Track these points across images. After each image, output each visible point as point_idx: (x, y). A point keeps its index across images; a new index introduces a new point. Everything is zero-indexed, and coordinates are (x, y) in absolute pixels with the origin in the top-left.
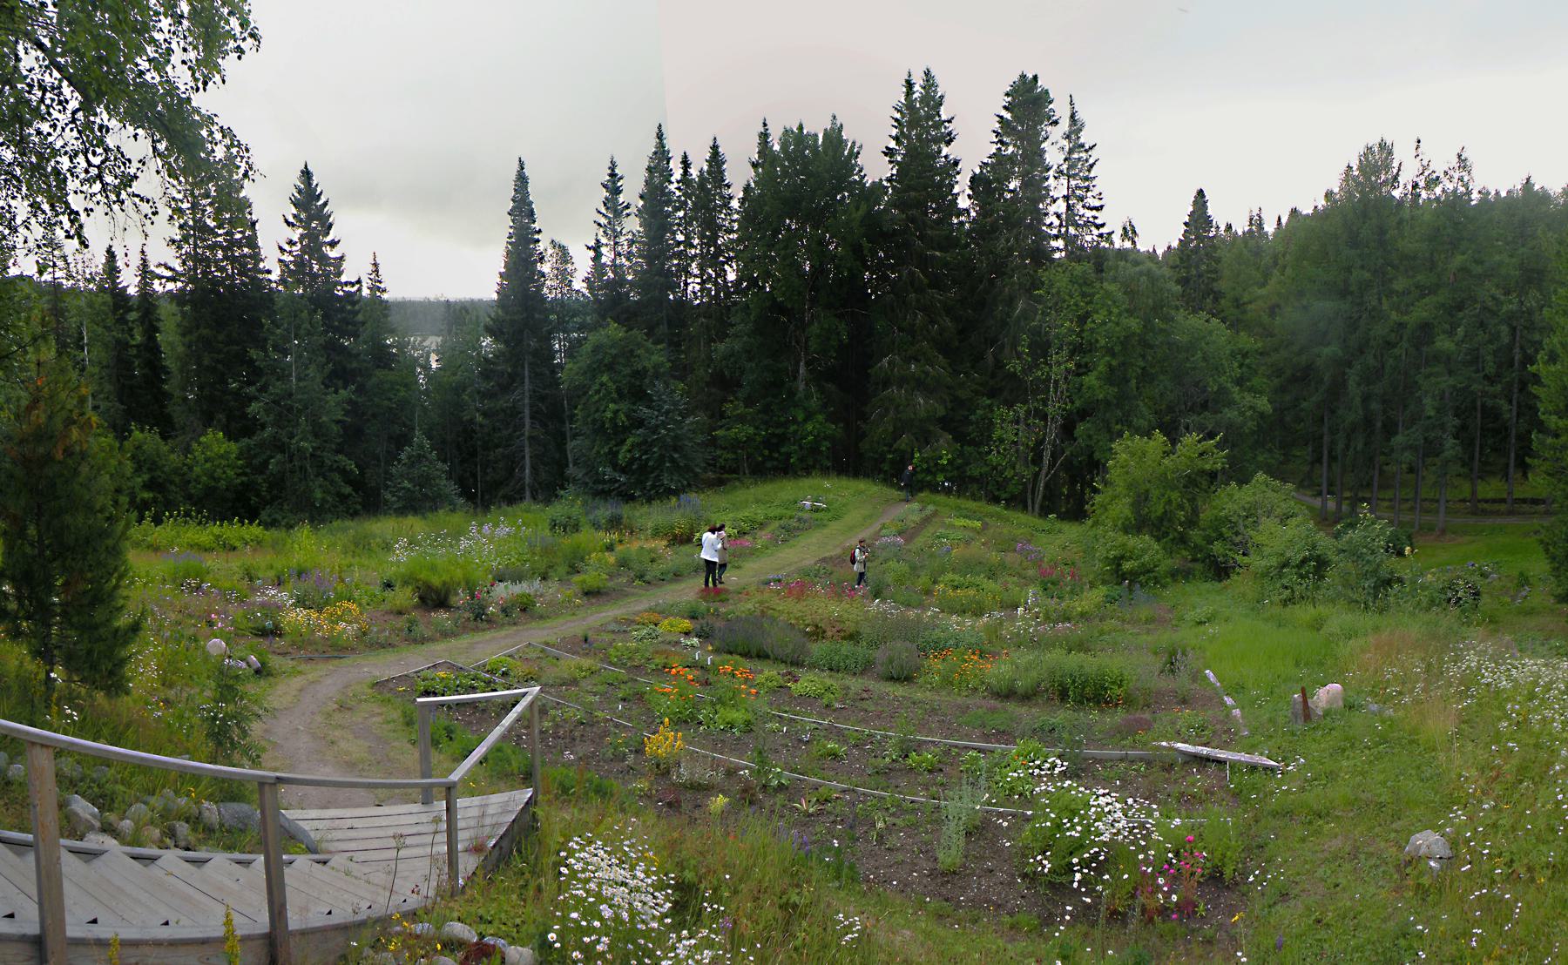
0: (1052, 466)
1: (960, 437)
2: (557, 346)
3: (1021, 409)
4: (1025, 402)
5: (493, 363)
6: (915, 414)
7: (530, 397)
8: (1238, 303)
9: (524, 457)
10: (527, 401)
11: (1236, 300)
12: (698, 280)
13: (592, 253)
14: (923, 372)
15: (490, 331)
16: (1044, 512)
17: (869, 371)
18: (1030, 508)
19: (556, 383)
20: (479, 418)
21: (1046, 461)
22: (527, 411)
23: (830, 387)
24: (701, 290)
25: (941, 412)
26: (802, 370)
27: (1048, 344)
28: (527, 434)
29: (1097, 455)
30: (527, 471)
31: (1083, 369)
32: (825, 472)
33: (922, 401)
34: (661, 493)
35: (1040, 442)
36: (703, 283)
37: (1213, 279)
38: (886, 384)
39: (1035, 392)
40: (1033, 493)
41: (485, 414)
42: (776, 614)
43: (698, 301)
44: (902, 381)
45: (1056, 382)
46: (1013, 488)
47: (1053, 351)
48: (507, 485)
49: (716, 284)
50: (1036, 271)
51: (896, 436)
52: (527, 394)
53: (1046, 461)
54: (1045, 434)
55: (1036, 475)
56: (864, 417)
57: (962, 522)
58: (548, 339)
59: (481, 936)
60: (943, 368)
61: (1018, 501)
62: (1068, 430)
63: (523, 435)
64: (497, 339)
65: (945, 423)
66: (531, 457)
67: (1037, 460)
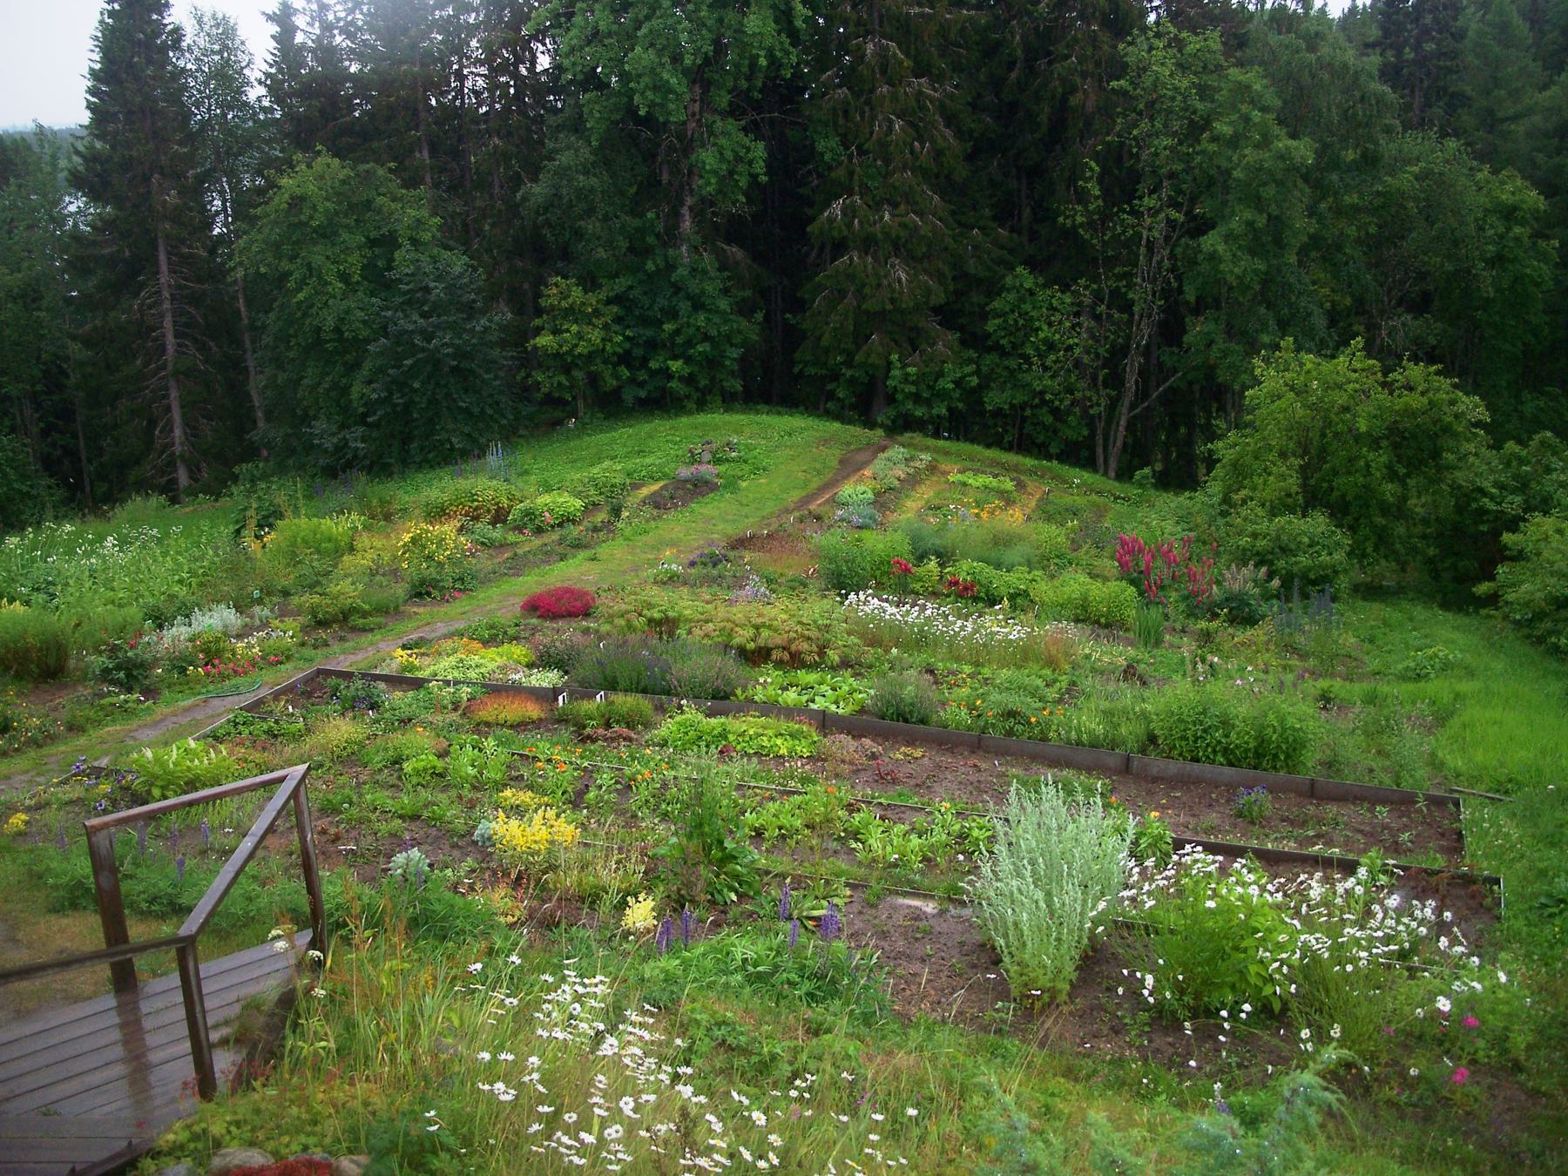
0: (1142, 394)
1: (975, 341)
2: (218, 203)
3: (1084, 290)
4: (1095, 279)
5: (94, 243)
6: (892, 301)
7: (173, 298)
8: (1491, 121)
9: (168, 409)
10: (167, 305)
11: (1490, 112)
12: (483, 70)
13: (274, 29)
14: (904, 226)
15: (78, 182)
16: (1124, 475)
17: (809, 229)
18: (1101, 461)
19: (217, 274)
20: (75, 349)
21: (1131, 381)
22: (168, 323)
23: (735, 252)
24: (491, 90)
25: (939, 298)
26: (687, 224)
27: (1135, 177)
28: (170, 367)
29: (1222, 376)
30: (178, 432)
31: (1200, 227)
32: (730, 401)
33: (903, 277)
34: (445, 457)
35: (1119, 353)
36: (494, 72)
37: (1450, 71)
38: (840, 247)
39: (1110, 262)
40: (1106, 440)
41: (87, 342)
42: (986, 869)
43: (484, 109)
44: (868, 244)
45: (1150, 245)
46: (1074, 430)
47: (1142, 188)
48: (765, 932)
49: (515, 75)
50: (1115, 47)
51: (861, 338)
52: (166, 294)
53: (1131, 381)
54: (1129, 337)
55: (1113, 404)
56: (799, 306)
57: (982, 480)
58: (195, 193)
59: (275, 1153)
60: (940, 220)
61: (1079, 454)
62: (1171, 331)
63: (164, 367)
64: (95, 195)
65: (947, 316)
66: (182, 407)
67: (1115, 380)
